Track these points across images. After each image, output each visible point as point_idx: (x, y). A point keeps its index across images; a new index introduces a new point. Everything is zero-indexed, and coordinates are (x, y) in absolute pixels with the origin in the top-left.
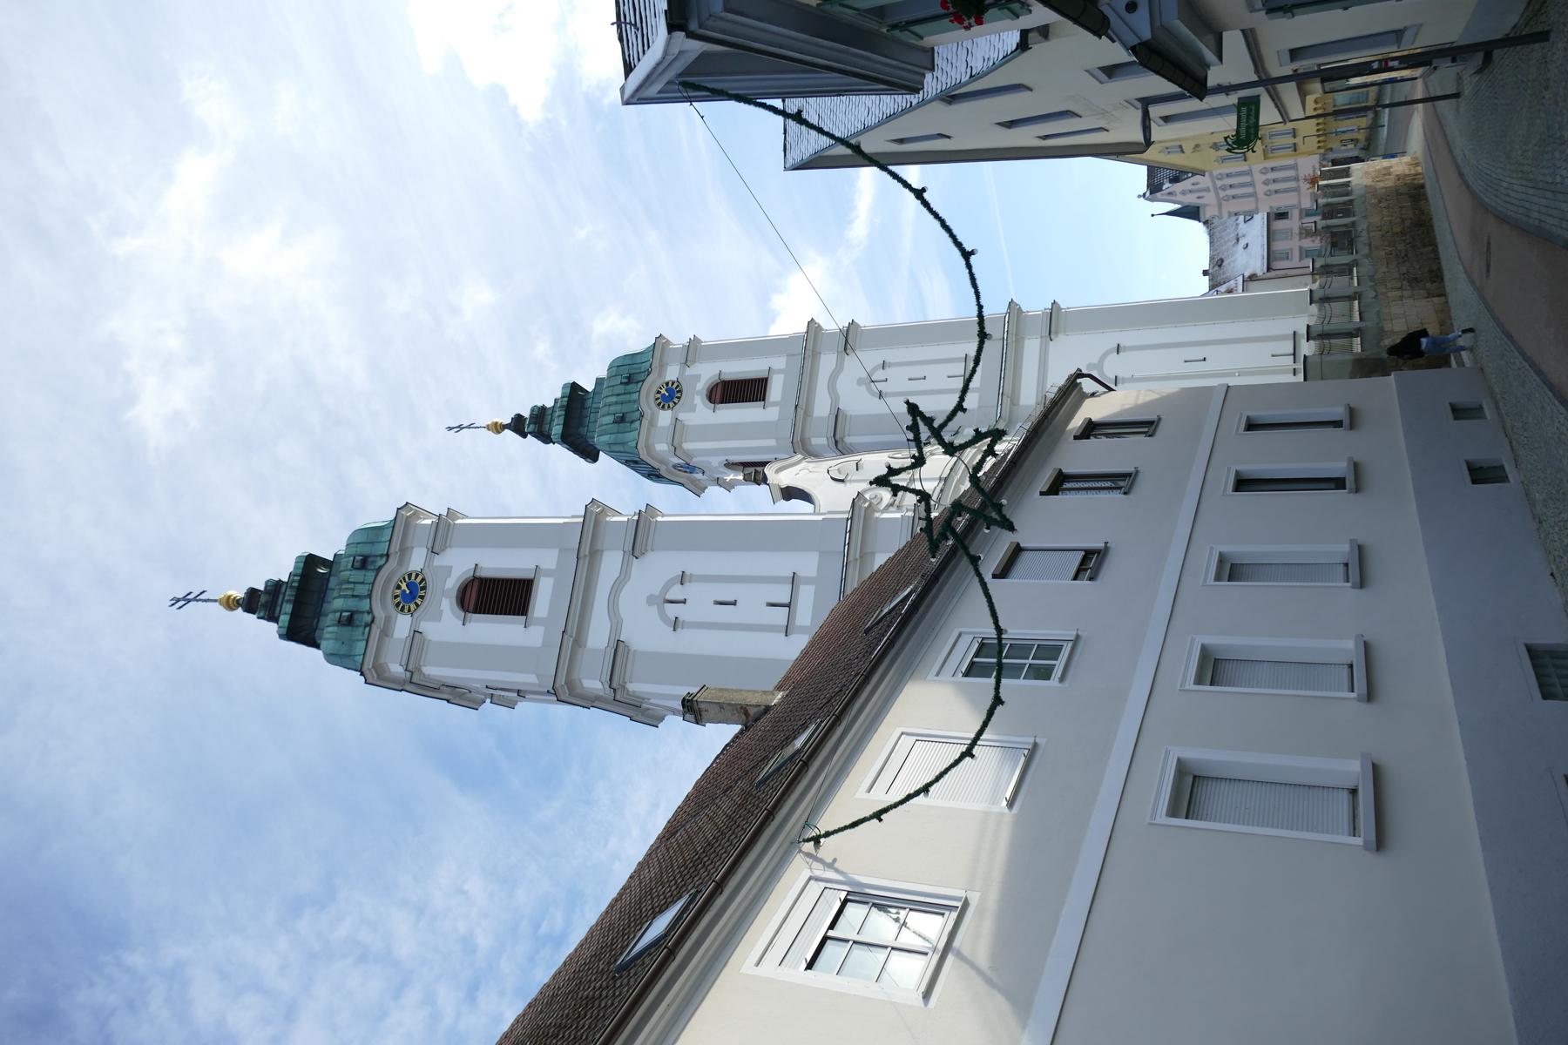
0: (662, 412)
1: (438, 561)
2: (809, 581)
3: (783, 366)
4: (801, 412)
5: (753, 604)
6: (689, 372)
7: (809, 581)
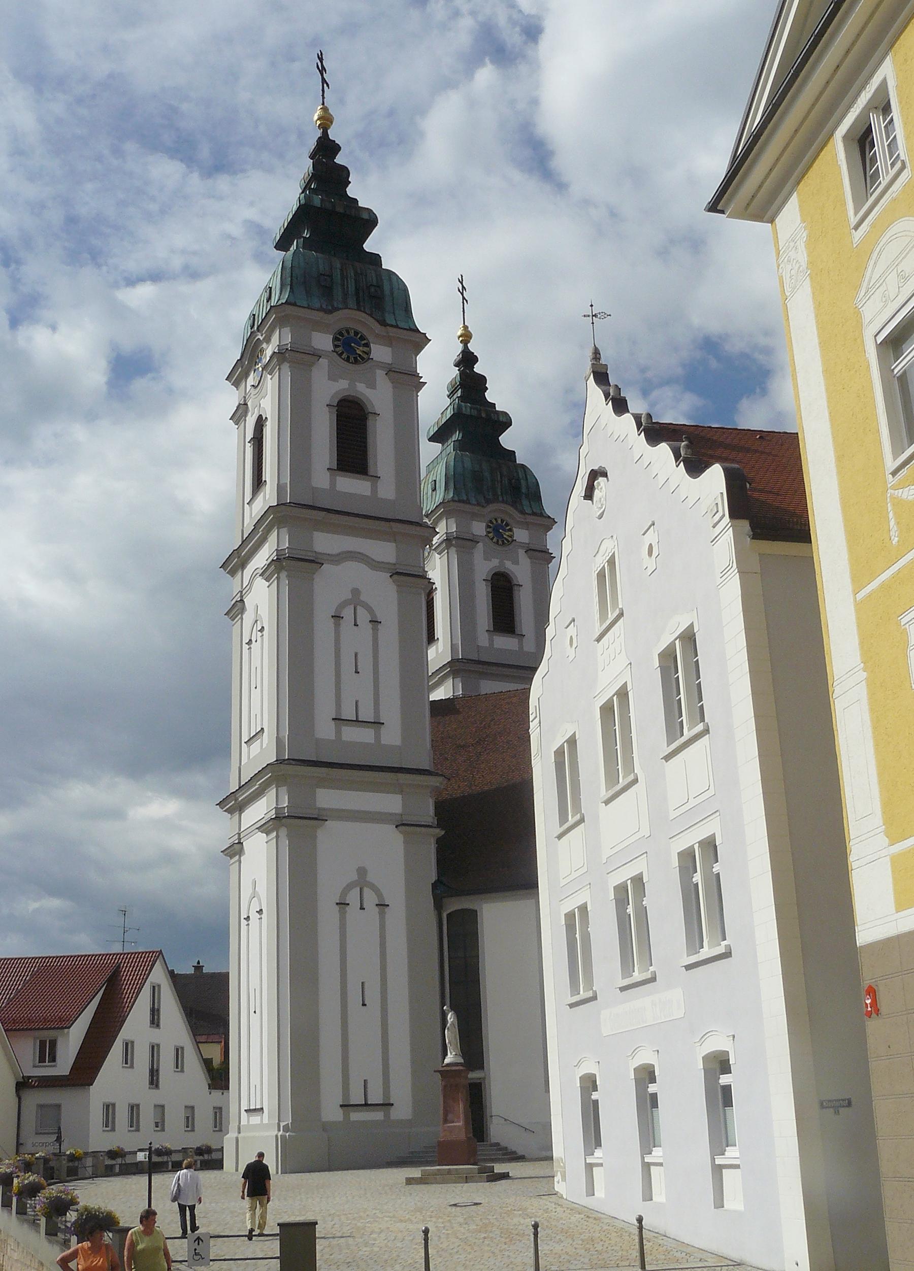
0: (330, 337)
1: (380, 374)
2: (378, 737)
3: (526, 649)
4: (479, 668)
5: (358, 693)
6: (521, 552)
7: (378, 737)
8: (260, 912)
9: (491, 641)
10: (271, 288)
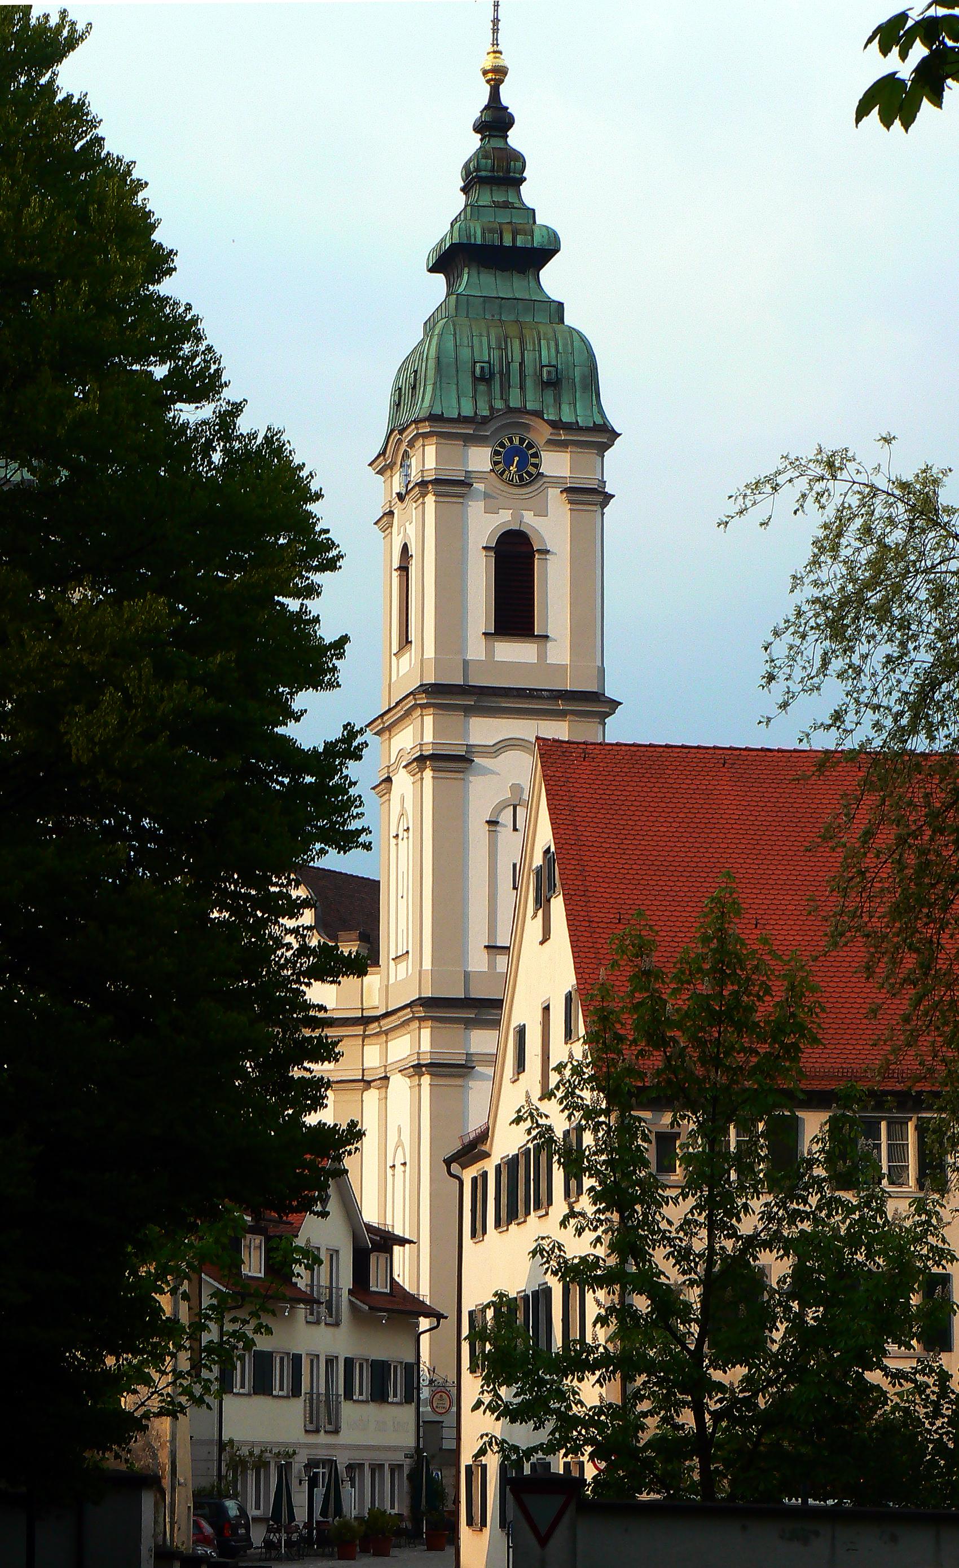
1: (554, 494)
8: (404, 1164)
9: (490, 652)
10: (400, 389)
